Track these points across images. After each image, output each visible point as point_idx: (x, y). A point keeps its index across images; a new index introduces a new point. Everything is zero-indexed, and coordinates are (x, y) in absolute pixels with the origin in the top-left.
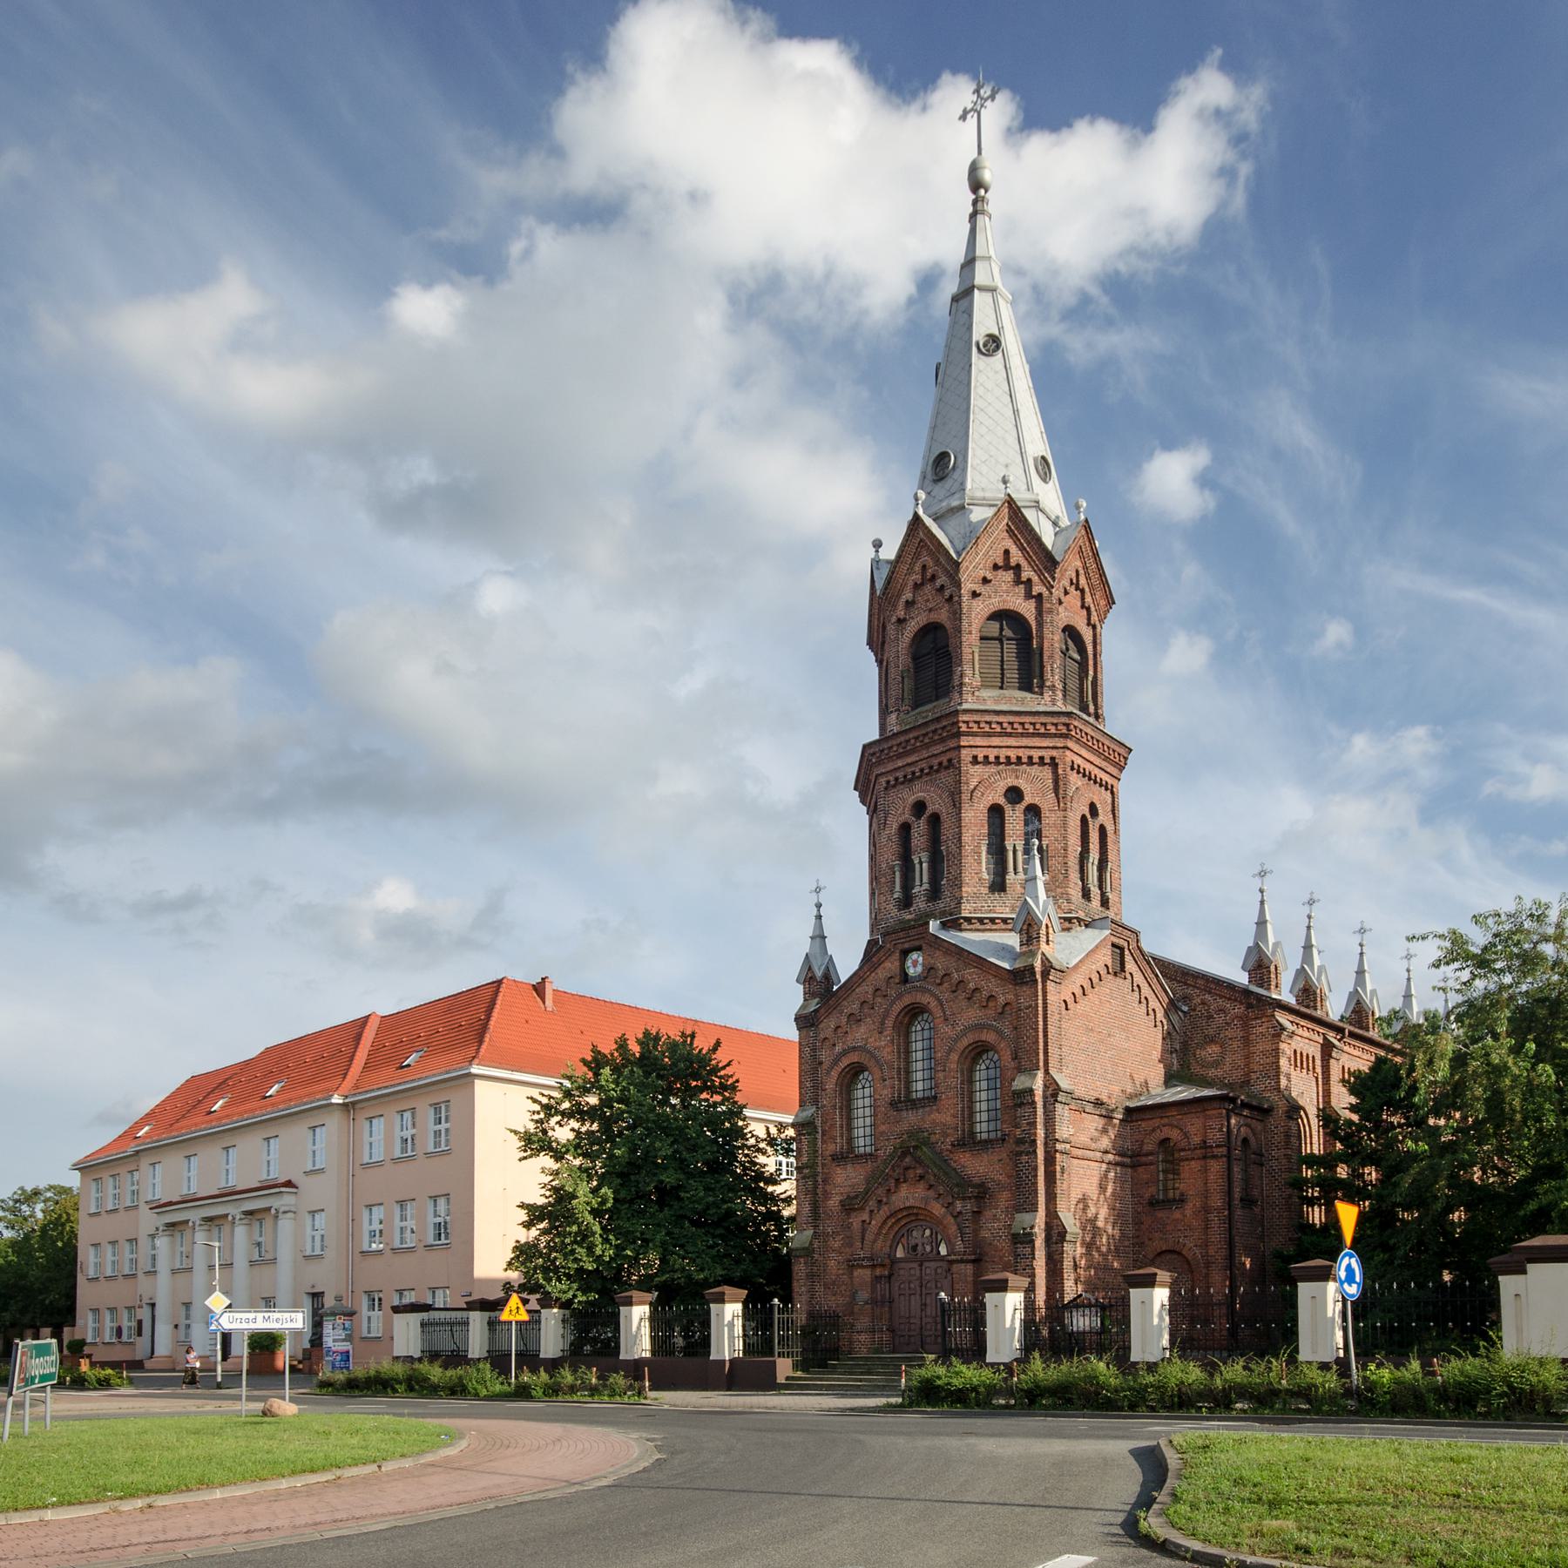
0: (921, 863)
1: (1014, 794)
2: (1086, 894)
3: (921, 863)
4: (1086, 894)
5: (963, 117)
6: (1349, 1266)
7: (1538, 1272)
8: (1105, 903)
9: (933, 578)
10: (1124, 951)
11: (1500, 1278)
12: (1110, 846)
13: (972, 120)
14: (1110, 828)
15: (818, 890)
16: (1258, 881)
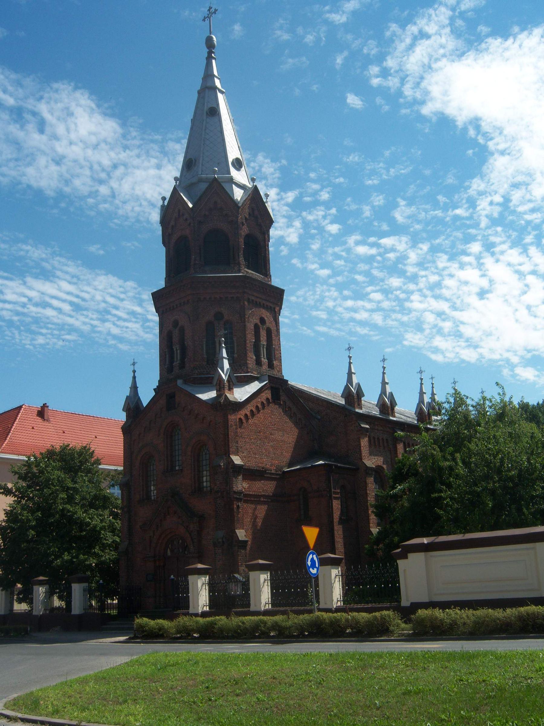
0: (177, 350)
1: (219, 316)
2: (259, 363)
3: (177, 350)
4: (259, 363)
5: (204, 20)
6: (313, 558)
7: (413, 557)
8: (271, 366)
9: (183, 215)
10: (280, 391)
11: (399, 562)
12: (274, 337)
13: (207, 21)
14: (273, 329)
15: (134, 364)
16: (347, 352)
